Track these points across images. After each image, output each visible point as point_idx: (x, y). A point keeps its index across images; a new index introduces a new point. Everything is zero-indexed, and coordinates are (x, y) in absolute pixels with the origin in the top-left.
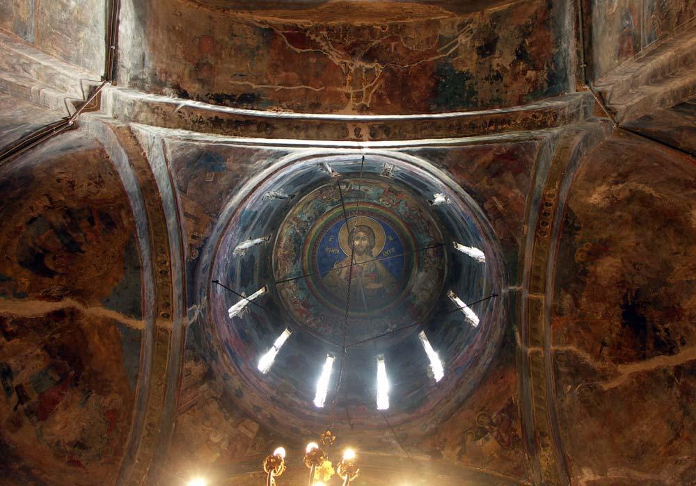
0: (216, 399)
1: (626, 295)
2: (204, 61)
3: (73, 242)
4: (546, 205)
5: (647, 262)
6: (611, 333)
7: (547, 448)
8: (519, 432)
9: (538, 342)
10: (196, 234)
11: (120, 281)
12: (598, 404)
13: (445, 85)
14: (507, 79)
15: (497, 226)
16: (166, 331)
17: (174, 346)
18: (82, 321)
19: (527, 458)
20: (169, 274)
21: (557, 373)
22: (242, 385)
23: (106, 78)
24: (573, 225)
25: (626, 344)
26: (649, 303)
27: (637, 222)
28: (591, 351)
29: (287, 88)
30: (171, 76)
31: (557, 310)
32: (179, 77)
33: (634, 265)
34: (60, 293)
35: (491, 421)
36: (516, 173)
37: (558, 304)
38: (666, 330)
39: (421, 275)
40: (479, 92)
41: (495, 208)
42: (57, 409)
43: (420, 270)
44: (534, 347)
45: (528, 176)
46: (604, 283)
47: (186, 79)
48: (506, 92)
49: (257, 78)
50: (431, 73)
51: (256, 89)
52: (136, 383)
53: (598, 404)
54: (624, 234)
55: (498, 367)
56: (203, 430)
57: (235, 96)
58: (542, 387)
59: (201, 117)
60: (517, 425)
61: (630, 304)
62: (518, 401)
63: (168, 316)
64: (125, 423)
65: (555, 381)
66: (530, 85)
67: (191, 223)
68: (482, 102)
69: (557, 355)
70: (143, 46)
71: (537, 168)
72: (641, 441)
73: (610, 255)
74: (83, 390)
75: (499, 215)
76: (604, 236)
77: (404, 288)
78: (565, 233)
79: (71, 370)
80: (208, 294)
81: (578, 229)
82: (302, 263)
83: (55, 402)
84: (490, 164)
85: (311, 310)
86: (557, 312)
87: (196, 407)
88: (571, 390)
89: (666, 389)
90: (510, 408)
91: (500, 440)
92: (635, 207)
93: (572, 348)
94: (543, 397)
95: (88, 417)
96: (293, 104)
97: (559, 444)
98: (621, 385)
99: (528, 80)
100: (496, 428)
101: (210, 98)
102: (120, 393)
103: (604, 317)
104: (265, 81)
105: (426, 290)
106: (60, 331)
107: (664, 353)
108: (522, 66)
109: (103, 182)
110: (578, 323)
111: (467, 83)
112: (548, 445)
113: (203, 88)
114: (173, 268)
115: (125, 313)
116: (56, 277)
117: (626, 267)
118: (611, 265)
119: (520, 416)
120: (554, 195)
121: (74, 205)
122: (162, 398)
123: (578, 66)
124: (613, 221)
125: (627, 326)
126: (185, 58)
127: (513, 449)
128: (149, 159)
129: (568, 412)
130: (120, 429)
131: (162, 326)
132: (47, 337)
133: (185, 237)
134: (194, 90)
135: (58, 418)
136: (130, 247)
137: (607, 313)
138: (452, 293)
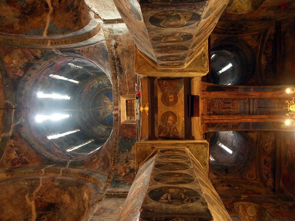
0: (29, 61)
1: (58, 205)
2: (130, 53)
3: (70, 9)
4: (88, 177)
5: (67, 212)
6: (46, 199)
7: (6, 176)
8: (17, 166)
9: (46, 173)
10: (83, 52)
11: (59, 27)
12: (20, 194)
13: (128, 142)
14: (125, 165)
15: (88, 159)
16: (47, 43)
17: (43, 46)
18: (45, 14)
19: (6, 169)
20: (65, 44)
21: (32, 180)
22: (39, 70)
23: (104, 20)
24: (79, 187)
25: (42, 204)
26: (54, 212)
27: (79, 209)
28: (39, 192)
29: (127, 84)
30: (120, 42)
31: (54, 180)
32: (121, 45)
33: (67, 208)
34: (54, 6)
35: (22, 156)
36: (103, 166)
37: (56, 180)
38: (44, 219)
39: (104, 130)
40: (123, 155)
41: (94, 159)
42: (12, 7)
43: (106, 129)
44: (44, 172)
45: (101, 171)
46: (62, 197)
47: (122, 47)
48: (120, 165)
49: (129, 73)
50: (133, 137)
51: (125, 72)
52: (24, 34)
53: (20, 194)
54: (76, 205)
55: (42, 159)
56: (17, 57)
57: (121, 65)
58: (30, 174)
59: (114, 53)
60: (20, 165)
61: (55, 206)
62: (28, 166)
63: (52, 44)
64: (9, 31)
65: (30, 179)
66: (119, 173)
67: (86, 50)
68: (119, 156)
69: (39, 179)
70: (125, 32)
71: (102, 174)
72: (4, 209)
73: (70, 199)
74: (20, 16)
75: (92, 160)
76: (76, 198)
77: (100, 123)
78: (77, 183)
79: (27, 11)
80: (68, 56)
81: (78, 189)
82: (107, 86)
83: (15, 6)
84: (107, 157)
85: (91, 90)
86: (53, 180)
87: (24, 54)
88: (26, 184)
89: (24, 218)
90: (26, 163)
91: (14, 160)
92: (82, 209)
93: (41, 185)
94: (26, 174)
95: (9, 18)
96: (121, 86)
97: (7, 180)
98: (27, 202)
99: (122, 173)
100: (19, 158)
101: (117, 56)
102: (20, 29)
103: (51, 196)
104: (128, 76)
105: (98, 131)
106: (41, 6)
107: (37, 217)
108: (128, 171)
109: (85, 19)
110: (49, 187)
111: (127, 150)
112: (8, 176)
113: (121, 53)
114: (68, 45)
115: (48, 29)
116: (59, 4)
117: (67, 205)
118: (67, 199)
119: (23, 166)
120: (91, 180)
121: (79, 9)
122: (23, 43)
123: (114, 192)
124: (79, 201)
125: (48, 204)
126: (129, 46)
127: (11, 164)
128: (96, 35)
129: (18, 183)
130: (6, 30)
131: (48, 42)
132: (38, 2)
133: (81, 48)
134: (118, 50)
135: (8, 8)
136: (69, 30)
137: (52, 198)
138: (93, 141)
